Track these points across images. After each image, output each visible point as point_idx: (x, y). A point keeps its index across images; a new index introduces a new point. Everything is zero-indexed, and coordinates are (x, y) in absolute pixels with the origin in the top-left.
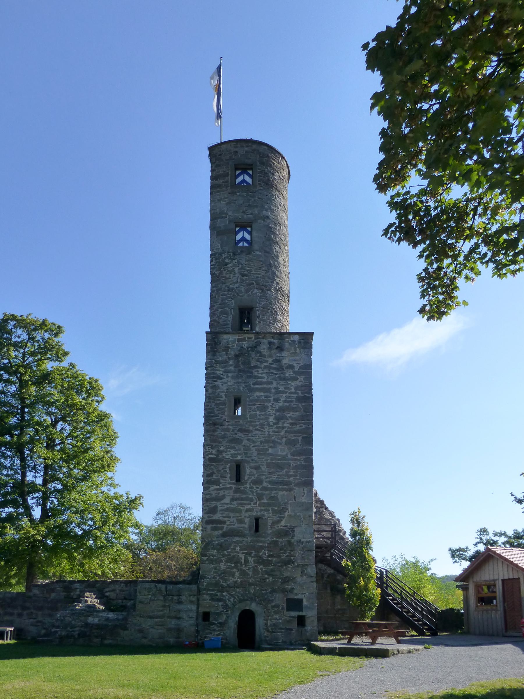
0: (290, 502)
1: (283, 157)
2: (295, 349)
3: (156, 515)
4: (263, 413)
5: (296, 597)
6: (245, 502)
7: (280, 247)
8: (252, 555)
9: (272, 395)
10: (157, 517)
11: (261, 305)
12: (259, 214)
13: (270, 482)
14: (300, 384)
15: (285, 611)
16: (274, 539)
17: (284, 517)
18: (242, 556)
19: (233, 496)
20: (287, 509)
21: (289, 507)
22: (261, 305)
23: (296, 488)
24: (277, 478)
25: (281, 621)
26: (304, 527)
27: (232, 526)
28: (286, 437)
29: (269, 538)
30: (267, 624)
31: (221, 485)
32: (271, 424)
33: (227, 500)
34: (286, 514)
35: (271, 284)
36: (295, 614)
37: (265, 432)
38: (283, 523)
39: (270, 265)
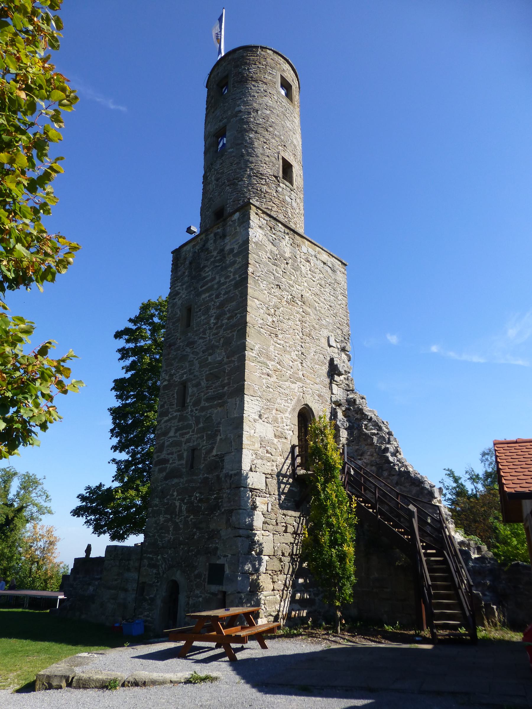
0: (223, 420)
1: (262, 48)
2: (236, 229)
3: (481, 456)
4: (206, 316)
5: (218, 562)
6: (184, 431)
7: (256, 132)
8: (185, 501)
9: (214, 292)
10: (484, 458)
11: (231, 200)
12: (232, 113)
13: (208, 400)
14: (240, 265)
15: (206, 584)
16: (206, 475)
17: (215, 443)
18: (177, 503)
19: (177, 426)
20: (219, 431)
21: (221, 428)
22: (231, 200)
23: (229, 400)
24: (214, 391)
25: (201, 599)
26: (233, 453)
27: (174, 465)
28: (223, 337)
29: (201, 476)
30: (188, 604)
31: (169, 416)
32: (212, 325)
33: (172, 434)
34: (219, 438)
35: (242, 173)
36: (214, 588)
37: (206, 338)
38: (214, 453)
39: (242, 155)
